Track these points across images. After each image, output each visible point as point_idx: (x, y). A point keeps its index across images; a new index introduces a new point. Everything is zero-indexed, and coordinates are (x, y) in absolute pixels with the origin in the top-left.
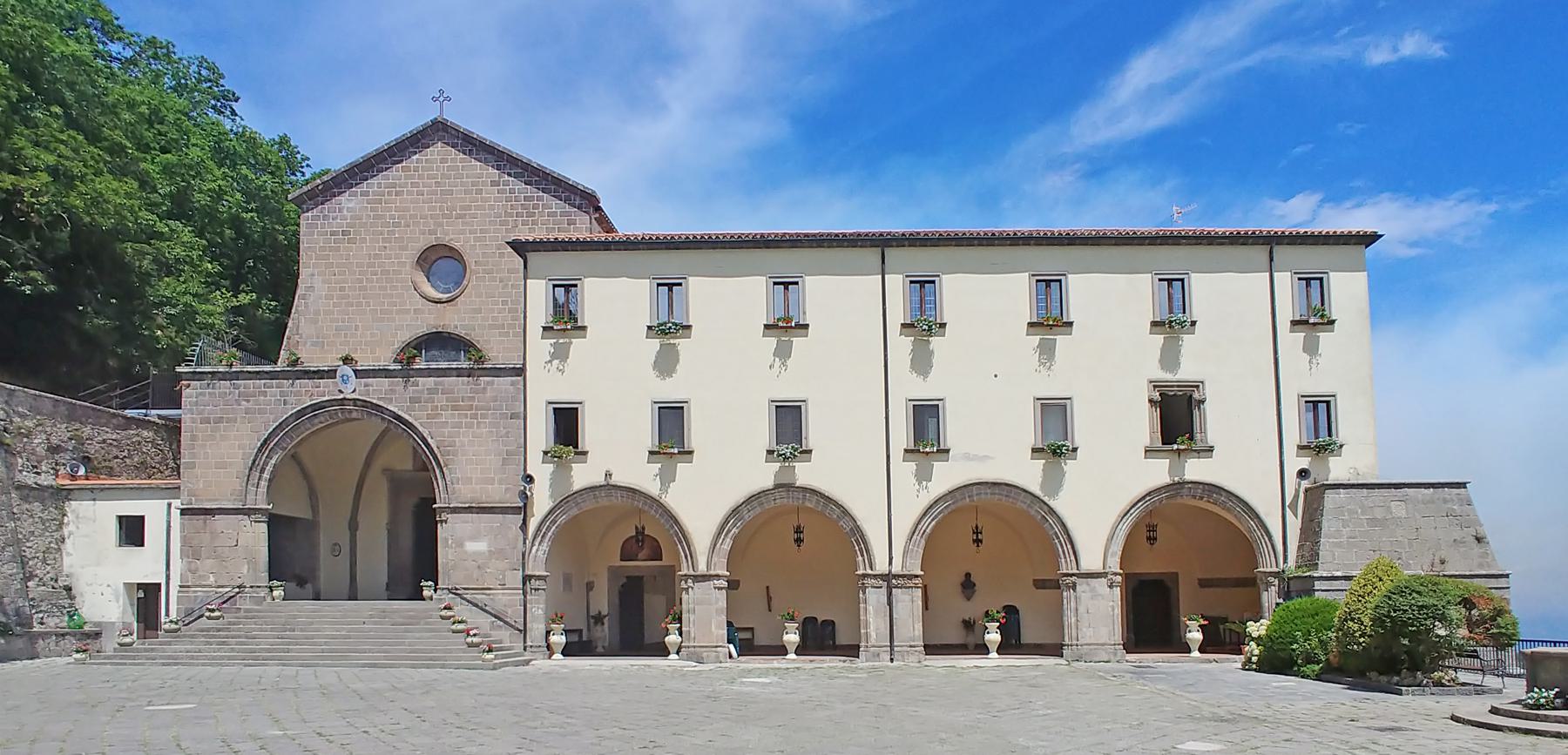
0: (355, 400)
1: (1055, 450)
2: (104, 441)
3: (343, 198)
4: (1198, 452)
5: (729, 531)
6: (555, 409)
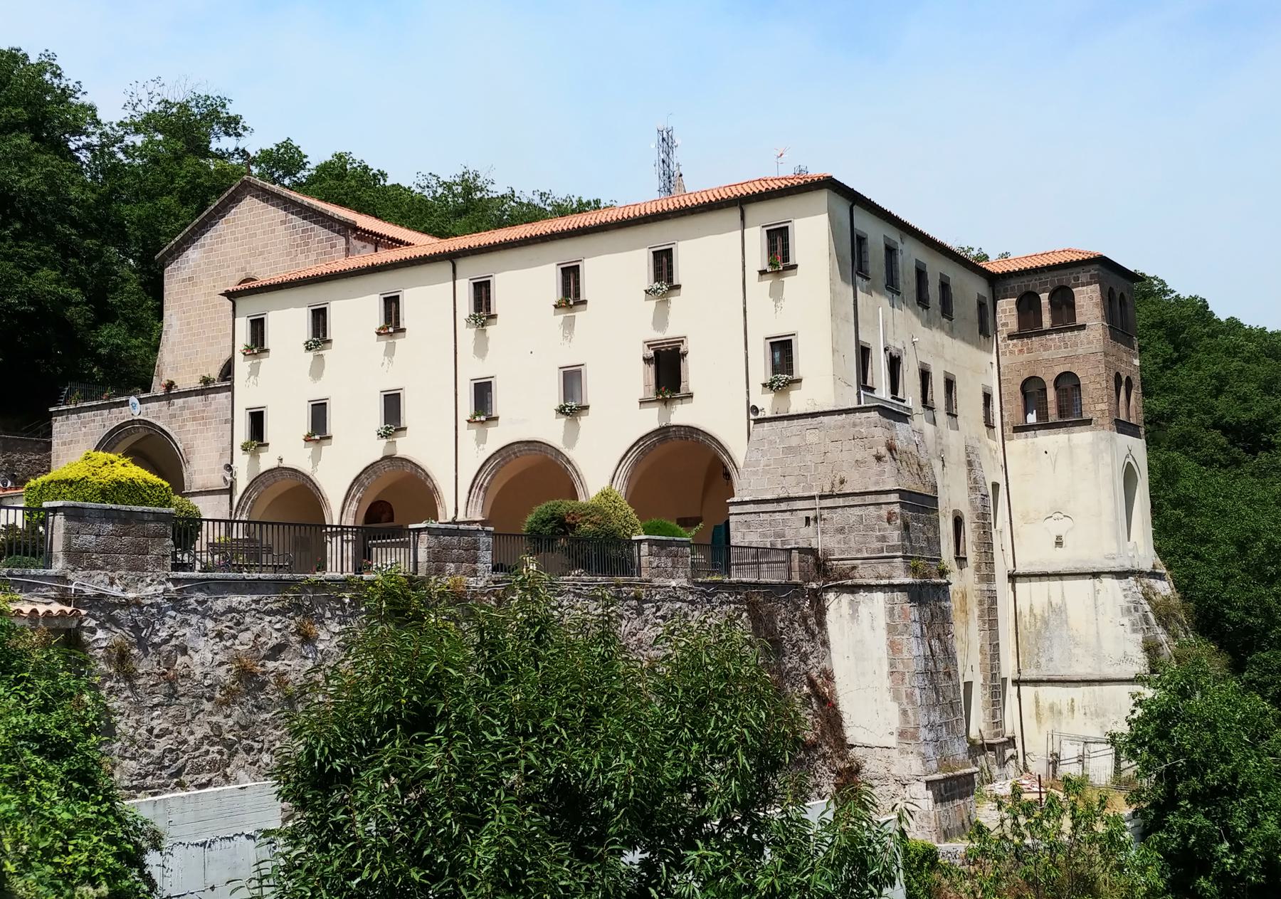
0: (139, 420)
1: (572, 409)
2: (30, 461)
3: (190, 252)
4: (681, 398)
5: (354, 496)
6: (771, 343)
